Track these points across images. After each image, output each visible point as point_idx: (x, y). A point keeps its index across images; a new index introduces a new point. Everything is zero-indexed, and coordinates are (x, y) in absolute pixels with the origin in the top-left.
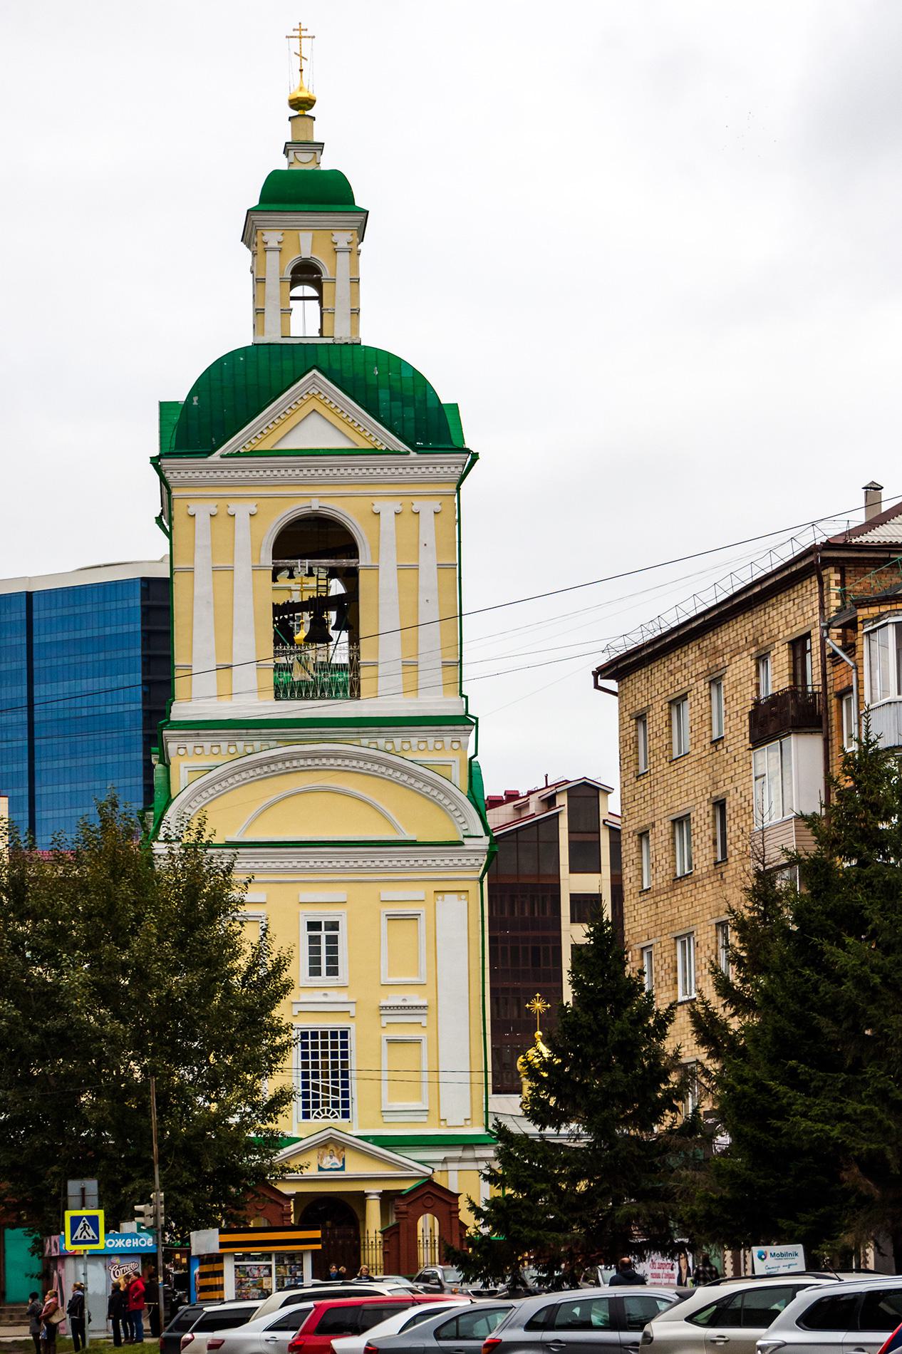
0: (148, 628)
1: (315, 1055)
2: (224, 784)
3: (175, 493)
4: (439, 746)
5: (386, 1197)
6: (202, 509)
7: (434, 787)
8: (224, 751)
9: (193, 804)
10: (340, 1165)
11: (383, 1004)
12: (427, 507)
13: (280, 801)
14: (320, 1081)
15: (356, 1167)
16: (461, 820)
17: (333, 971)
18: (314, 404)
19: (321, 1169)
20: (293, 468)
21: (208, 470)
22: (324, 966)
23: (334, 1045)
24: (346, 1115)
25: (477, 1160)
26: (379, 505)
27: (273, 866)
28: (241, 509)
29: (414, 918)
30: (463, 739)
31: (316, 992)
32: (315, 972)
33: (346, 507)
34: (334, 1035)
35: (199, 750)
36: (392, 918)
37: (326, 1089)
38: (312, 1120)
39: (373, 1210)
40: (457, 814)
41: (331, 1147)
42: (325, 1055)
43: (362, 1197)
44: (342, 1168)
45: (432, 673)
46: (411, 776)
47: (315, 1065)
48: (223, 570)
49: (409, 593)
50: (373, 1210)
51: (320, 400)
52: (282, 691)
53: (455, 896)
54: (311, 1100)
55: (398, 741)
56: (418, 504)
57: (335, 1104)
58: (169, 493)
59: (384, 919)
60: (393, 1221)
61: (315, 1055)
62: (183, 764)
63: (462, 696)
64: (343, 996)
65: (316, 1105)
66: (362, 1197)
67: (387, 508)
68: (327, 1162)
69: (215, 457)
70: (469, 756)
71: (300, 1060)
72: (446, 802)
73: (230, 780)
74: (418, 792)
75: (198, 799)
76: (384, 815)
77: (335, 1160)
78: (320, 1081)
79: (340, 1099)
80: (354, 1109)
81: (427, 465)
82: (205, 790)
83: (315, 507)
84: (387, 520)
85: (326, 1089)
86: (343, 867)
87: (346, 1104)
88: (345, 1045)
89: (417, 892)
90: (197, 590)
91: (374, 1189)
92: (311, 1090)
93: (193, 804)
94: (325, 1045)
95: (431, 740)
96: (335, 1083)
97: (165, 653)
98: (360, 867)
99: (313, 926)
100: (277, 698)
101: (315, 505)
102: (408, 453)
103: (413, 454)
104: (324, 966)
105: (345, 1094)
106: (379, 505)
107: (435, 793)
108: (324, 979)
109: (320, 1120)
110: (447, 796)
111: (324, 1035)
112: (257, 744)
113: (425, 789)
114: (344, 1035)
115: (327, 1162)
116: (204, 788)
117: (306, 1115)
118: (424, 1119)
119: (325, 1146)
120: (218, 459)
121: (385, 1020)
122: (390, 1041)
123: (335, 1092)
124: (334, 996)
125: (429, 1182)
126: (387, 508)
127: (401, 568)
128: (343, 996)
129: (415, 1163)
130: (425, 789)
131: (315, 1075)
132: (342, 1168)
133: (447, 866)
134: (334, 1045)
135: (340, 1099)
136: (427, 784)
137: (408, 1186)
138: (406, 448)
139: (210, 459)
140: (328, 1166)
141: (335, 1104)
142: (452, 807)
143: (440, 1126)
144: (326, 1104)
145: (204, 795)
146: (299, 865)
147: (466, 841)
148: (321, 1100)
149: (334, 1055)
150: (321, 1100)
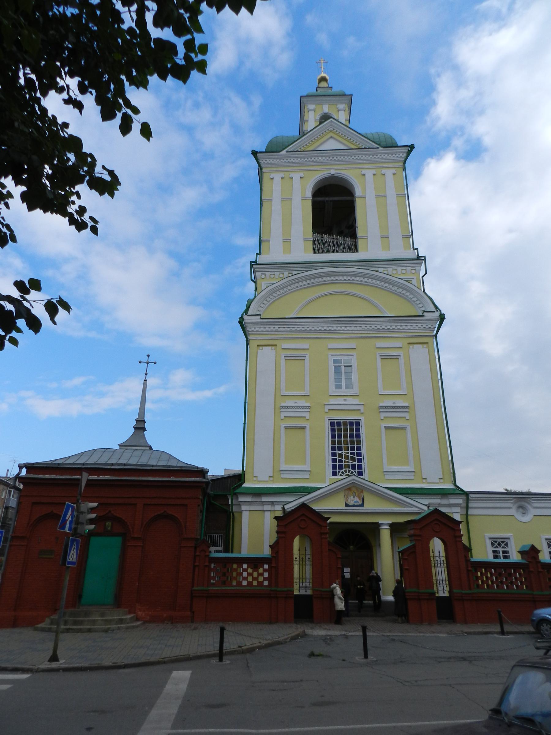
1: (340, 436)
2: (285, 289)
3: (264, 170)
4: (404, 271)
5: (395, 528)
6: (277, 177)
7: (404, 289)
8: (277, 277)
9: (268, 299)
10: (360, 503)
11: (381, 405)
12: (389, 173)
13: (321, 297)
16: (421, 306)
18: (331, 134)
19: (347, 505)
20: (322, 157)
21: (283, 158)
23: (351, 430)
24: (360, 474)
25: (273, 503)
27: (313, 329)
28: (296, 176)
29: (396, 357)
30: (417, 268)
31: (339, 398)
32: (338, 386)
33: (351, 174)
34: (351, 424)
35: (272, 276)
36: (383, 357)
37: (347, 457)
38: (339, 477)
39: (385, 535)
40: (418, 302)
41: (354, 489)
42: (345, 436)
43: (376, 527)
44: (362, 505)
45: (396, 239)
46: (390, 284)
47: (340, 442)
48: (287, 200)
49: (383, 215)
50: (385, 535)
51: (334, 133)
54: (356, 451)
55: (390, 270)
57: (353, 467)
58: (261, 169)
59: (379, 358)
60: (406, 544)
61: (340, 436)
63: (414, 249)
64: (356, 401)
65: (341, 467)
66: (376, 527)
68: (352, 500)
69: (284, 152)
70: (421, 275)
71: (330, 439)
72: (411, 296)
73: (289, 288)
75: (271, 297)
77: (357, 499)
78: (343, 452)
79: (356, 463)
80: (366, 470)
81: (388, 154)
82: (275, 292)
85: (347, 457)
86: (353, 330)
87: (360, 467)
89: (398, 343)
90: (273, 208)
91: (385, 521)
92: (337, 458)
93: (268, 299)
94: (345, 430)
95: (399, 269)
96: (353, 454)
98: (364, 330)
100: (315, 252)
101: (333, 172)
102: (378, 148)
103: (381, 148)
105: (360, 461)
107: (404, 292)
110: (411, 293)
111: (345, 424)
113: (393, 289)
114: (358, 424)
115: (352, 500)
117: (335, 474)
118: (412, 477)
119: (349, 489)
120: (285, 153)
121: (383, 415)
122: (387, 428)
123: (353, 459)
124: (350, 400)
125: (436, 511)
126: (369, 173)
127: (377, 196)
128: (356, 401)
129: (422, 505)
130: (398, 291)
131: (340, 448)
132: (362, 505)
133: (414, 329)
134: (351, 430)
135: (356, 463)
136: (399, 287)
137: (465, 540)
138: (378, 146)
139: (281, 153)
140: (352, 503)
141: (353, 467)
142: (415, 299)
143: (423, 483)
144: (348, 466)
145: (274, 295)
146: (328, 329)
147: (425, 314)
148: (344, 464)
149: (352, 436)
150: (344, 464)
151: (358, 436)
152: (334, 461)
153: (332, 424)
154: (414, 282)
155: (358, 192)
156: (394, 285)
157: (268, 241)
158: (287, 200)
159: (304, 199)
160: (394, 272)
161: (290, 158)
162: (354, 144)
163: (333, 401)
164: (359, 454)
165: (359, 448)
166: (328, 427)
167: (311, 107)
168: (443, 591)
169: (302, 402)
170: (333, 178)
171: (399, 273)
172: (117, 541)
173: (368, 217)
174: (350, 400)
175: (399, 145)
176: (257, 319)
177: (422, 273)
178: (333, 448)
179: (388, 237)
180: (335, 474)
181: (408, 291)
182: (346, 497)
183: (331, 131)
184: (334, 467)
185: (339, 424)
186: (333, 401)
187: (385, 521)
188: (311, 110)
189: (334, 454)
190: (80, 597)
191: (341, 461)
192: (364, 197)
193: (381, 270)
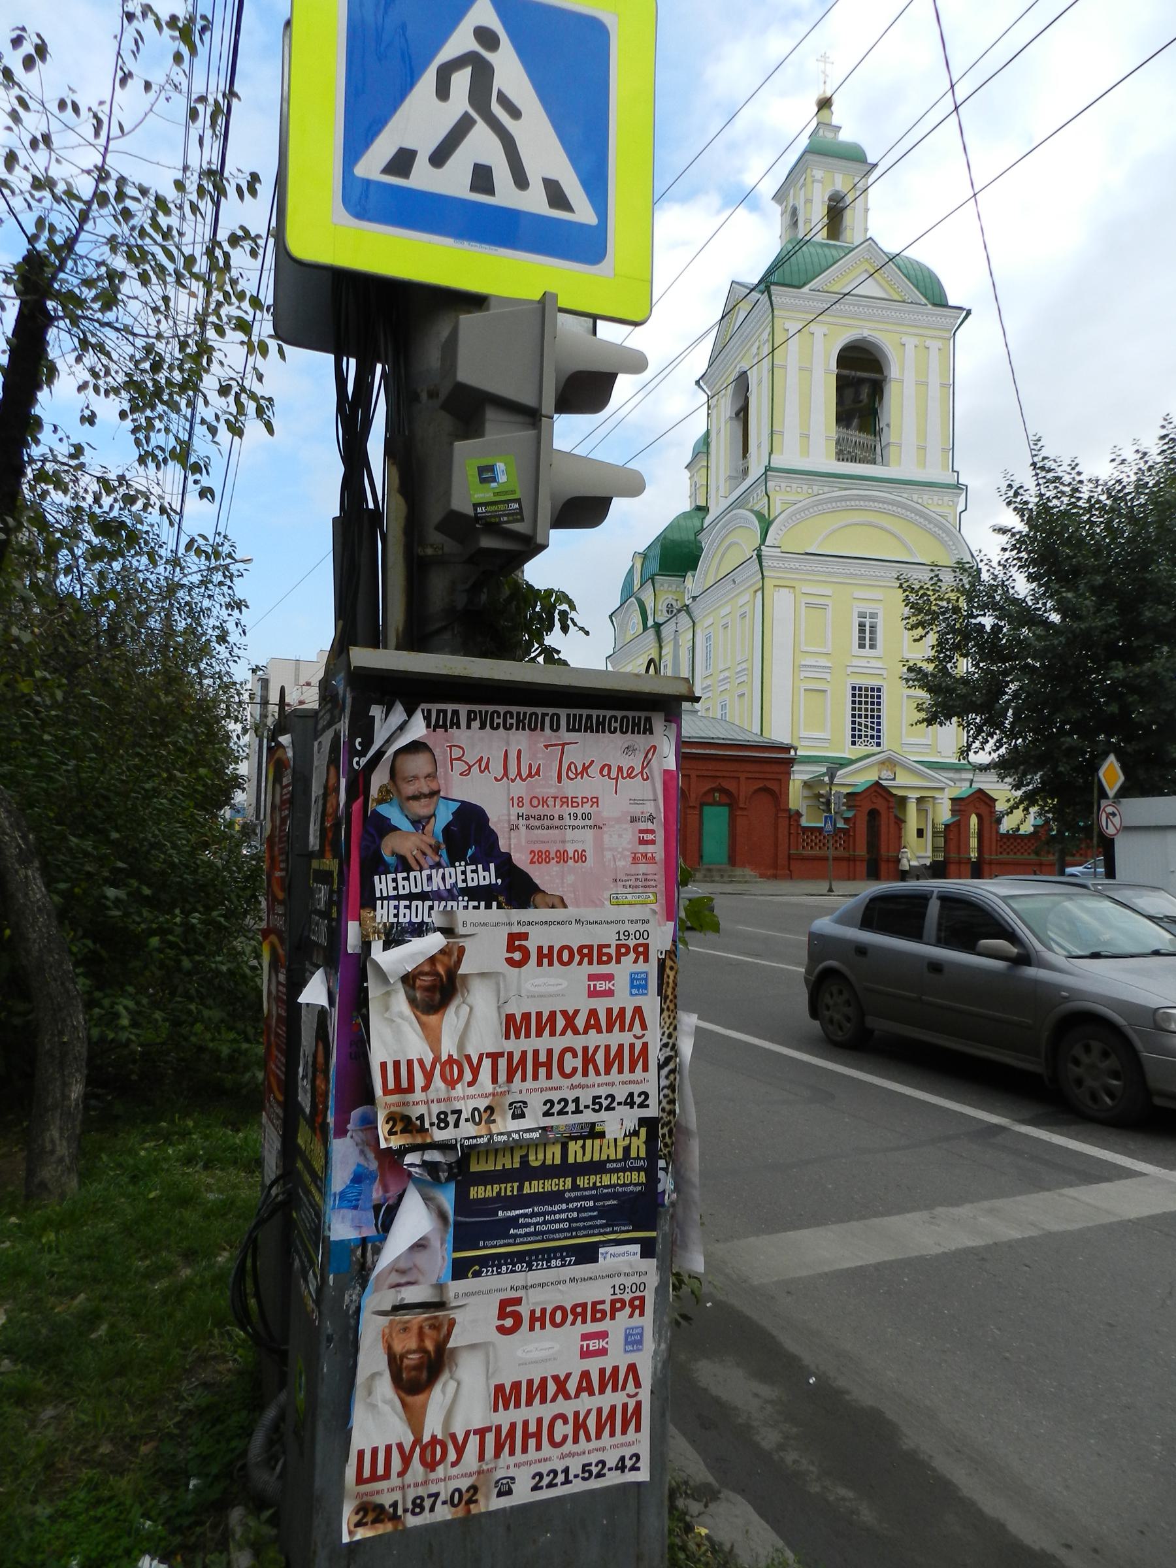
0: (845, 372)
3: (776, 312)
12: (934, 344)
13: (862, 524)
14: (863, 720)
15: (903, 779)
17: (872, 647)
22: (867, 642)
24: (879, 744)
26: (905, 339)
29: (823, 607)
32: (862, 646)
34: (872, 690)
38: (857, 747)
43: (903, 800)
44: (894, 779)
46: (926, 519)
48: (806, 370)
52: (841, 456)
53: (787, 590)
55: (925, 497)
56: (929, 342)
57: (872, 737)
62: (778, 498)
65: (860, 737)
67: (911, 342)
69: (806, 289)
70: (959, 510)
74: (928, 531)
76: (904, 544)
80: (884, 740)
83: (865, 335)
84: (910, 347)
87: (879, 737)
88: (879, 697)
91: (913, 795)
94: (866, 696)
97: (845, 372)
99: (862, 615)
101: (866, 333)
103: (930, 306)
104: (867, 642)
105: (879, 731)
106: (905, 339)
108: (867, 651)
109: (863, 747)
111: (866, 689)
112: (826, 489)
114: (879, 690)
116: (794, 514)
124: (874, 663)
126: (911, 342)
131: (860, 716)
132: (894, 779)
136: (936, 525)
138: (924, 301)
141: (872, 737)
144: (866, 736)
149: (872, 703)
151: (879, 704)
152: (853, 729)
153: (854, 688)
154: (950, 519)
155: (894, 371)
156: (930, 522)
157: (782, 433)
158: (806, 370)
159: (827, 371)
160: (930, 501)
161: (814, 300)
162: (898, 293)
163: (856, 662)
164: (879, 724)
165: (879, 717)
166: (850, 692)
167: (818, 174)
168: (974, 855)
169: (823, 662)
170: (864, 340)
171: (933, 503)
172: (724, 811)
173: (901, 406)
174: (874, 663)
175: (950, 303)
176: (776, 552)
177: (961, 507)
178: (853, 716)
179: (925, 448)
180: (854, 743)
181: (944, 531)
182: (880, 771)
183: (867, 260)
184: (853, 736)
185: (860, 689)
186: (856, 662)
187: (913, 795)
188: (818, 181)
189: (853, 723)
190: (701, 857)
191: (860, 730)
192: (902, 381)
193: (915, 497)
